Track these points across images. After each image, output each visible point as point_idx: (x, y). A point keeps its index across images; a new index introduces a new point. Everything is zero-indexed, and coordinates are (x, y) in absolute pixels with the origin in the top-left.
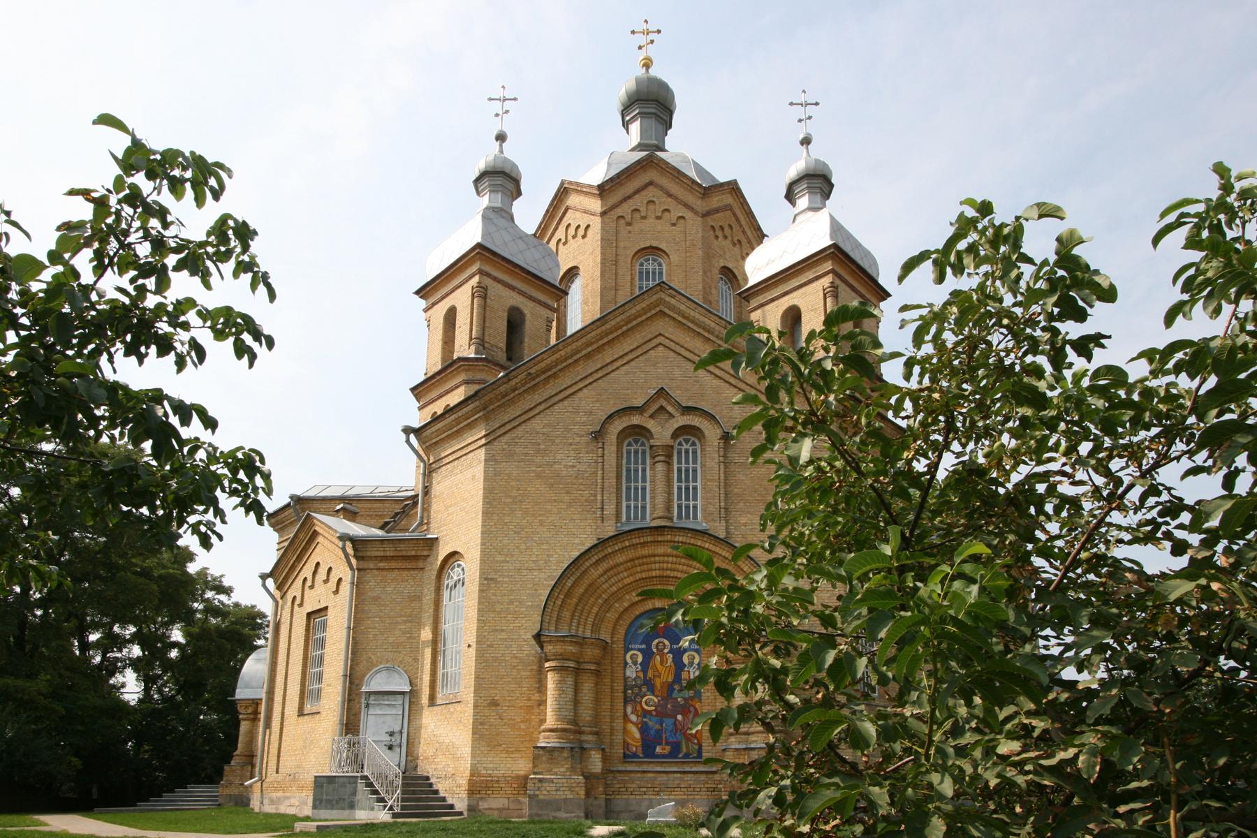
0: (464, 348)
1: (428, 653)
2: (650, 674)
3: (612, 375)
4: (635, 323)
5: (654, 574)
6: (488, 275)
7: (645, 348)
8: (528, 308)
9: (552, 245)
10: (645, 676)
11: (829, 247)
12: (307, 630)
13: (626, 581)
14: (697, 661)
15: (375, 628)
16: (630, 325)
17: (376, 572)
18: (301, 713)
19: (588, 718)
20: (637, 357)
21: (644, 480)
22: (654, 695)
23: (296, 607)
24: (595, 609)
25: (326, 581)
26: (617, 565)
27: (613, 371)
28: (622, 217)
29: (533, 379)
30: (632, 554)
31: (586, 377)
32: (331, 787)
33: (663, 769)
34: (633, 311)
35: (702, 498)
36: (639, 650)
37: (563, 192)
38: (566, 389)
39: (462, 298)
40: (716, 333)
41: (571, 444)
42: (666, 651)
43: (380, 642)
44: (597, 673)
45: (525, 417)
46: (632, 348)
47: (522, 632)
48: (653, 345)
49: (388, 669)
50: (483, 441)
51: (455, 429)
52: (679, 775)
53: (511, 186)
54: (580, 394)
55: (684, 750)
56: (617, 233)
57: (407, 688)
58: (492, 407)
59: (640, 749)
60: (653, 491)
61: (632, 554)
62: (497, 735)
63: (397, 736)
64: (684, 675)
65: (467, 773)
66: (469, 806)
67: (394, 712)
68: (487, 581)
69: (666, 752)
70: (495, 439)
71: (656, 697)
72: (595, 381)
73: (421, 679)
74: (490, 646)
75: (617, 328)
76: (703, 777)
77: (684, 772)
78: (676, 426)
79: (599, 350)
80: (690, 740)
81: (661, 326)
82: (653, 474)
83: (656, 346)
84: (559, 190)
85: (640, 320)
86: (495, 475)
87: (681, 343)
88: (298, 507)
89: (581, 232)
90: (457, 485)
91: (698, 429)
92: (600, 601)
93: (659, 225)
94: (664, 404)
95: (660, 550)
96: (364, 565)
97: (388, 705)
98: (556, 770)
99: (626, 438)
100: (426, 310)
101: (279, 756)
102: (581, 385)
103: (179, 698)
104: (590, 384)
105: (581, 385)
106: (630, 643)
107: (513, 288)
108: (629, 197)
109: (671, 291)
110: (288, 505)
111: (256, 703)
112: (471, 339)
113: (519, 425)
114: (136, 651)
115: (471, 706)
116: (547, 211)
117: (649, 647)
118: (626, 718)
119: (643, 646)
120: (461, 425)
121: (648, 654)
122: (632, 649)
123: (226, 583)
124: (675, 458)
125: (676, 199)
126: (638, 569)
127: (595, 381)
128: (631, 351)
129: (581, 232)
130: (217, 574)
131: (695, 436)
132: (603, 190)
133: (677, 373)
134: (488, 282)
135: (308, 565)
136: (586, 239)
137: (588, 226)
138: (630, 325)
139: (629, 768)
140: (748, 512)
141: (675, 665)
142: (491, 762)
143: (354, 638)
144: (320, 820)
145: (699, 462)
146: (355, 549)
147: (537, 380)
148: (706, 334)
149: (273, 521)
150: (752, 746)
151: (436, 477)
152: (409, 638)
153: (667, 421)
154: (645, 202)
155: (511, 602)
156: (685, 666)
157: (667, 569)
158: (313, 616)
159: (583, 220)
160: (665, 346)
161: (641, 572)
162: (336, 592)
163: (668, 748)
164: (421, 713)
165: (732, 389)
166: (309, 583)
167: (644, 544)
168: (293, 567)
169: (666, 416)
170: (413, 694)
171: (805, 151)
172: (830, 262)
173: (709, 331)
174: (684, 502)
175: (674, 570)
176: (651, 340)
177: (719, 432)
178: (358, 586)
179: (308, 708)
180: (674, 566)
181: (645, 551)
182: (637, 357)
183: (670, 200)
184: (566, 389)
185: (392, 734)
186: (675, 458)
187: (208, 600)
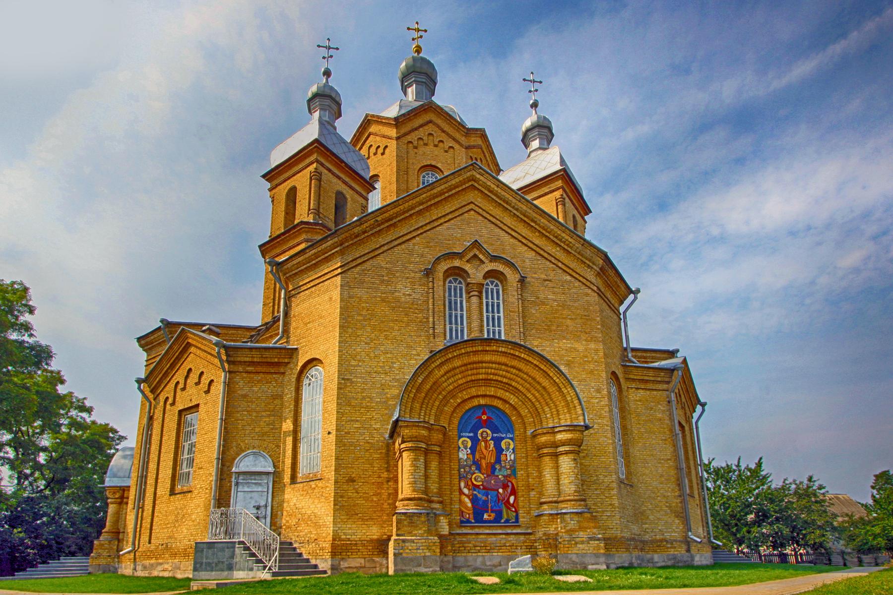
0: (303, 214)
1: (289, 440)
2: (477, 456)
3: (437, 229)
4: (454, 191)
5: (481, 377)
6: (322, 165)
7: (461, 211)
8: (349, 194)
9: (364, 152)
10: (474, 457)
11: (560, 171)
12: (179, 424)
13: (460, 382)
14: (512, 447)
15: (243, 420)
16: (451, 193)
17: (245, 375)
18: (172, 492)
19: (435, 490)
20: (455, 217)
21: (462, 310)
22: (480, 472)
23: (168, 407)
24: (437, 403)
25: (198, 384)
26: (454, 368)
27: (438, 226)
28: (411, 142)
29: (379, 225)
30: (466, 360)
31: (418, 229)
32: (210, 551)
33: (491, 532)
34: (453, 182)
35: (505, 325)
36: (468, 437)
37: (368, 122)
38: (403, 236)
39: (302, 181)
40: (513, 204)
41: (408, 278)
42: (489, 438)
43: (247, 432)
44: (440, 454)
45: (372, 255)
46: (451, 210)
47: (373, 422)
48: (467, 210)
49: (254, 453)
50: (339, 271)
51: (314, 262)
52: (504, 536)
53: (335, 107)
54: (414, 241)
55: (505, 516)
56: (408, 152)
57: (271, 469)
58: (347, 244)
59: (472, 516)
60: (469, 318)
61: (466, 360)
62: (354, 506)
63: (263, 509)
64: (503, 458)
65: (330, 538)
66: (332, 565)
67: (260, 489)
68: (344, 382)
69: (492, 518)
70: (348, 269)
71: (483, 474)
72: (425, 232)
73: (283, 462)
74: (348, 433)
75: (442, 193)
76: (522, 538)
77: (507, 534)
78: (486, 270)
79: (428, 209)
80: (510, 509)
81: (471, 196)
82: (467, 305)
83: (469, 211)
84: (364, 121)
85: (457, 190)
86: (350, 297)
87: (486, 210)
88: (167, 330)
89: (380, 151)
90: (315, 305)
91: (502, 273)
92: (440, 397)
93: (436, 151)
94: (477, 253)
95: (487, 358)
96: (235, 368)
97: (255, 484)
98: (416, 532)
99: (448, 277)
100: (270, 190)
101: (151, 529)
102: (415, 234)
103: (47, 492)
104: (421, 234)
105: (415, 234)
106: (461, 432)
107: (339, 178)
108: (416, 129)
109: (480, 170)
110: (159, 329)
111: (124, 490)
112: (309, 210)
113: (367, 260)
114: (11, 454)
115: (332, 482)
116: (355, 135)
117: (476, 434)
118: (461, 492)
119: (471, 434)
120: (319, 259)
121: (475, 441)
122: (463, 437)
123: (88, 404)
124: (484, 294)
125: (448, 134)
126: (470, 372)
127: (425, 232)
128: (451, 212)
129: (380, 151)
130: (81, 397)
131: (498, 279)
132: (398, 122)
133: (484, 231)
134: (321, 169)
135: (180, 371)
136: (384, 156)
137: (386, 147)
138: (451, 193)
139: (465, 531)
140: (539, 338)
141: (496, 449)
142: (350, 529)
143: (225, 428)
144: (218, 580)
145: (501, 298)
146: (228, 355)
147: (382, 227)
148: (505, 205)
149: (143, 342)
150: (563, 511)
151: (295, 302)
152: (272, 429)
153: (479, 266)
154: (427, 133)
155: (364, 398)
156: (503, 450)
157: (491, 374)
158: (184, 413)
159: (383, 142)
160: (475, 211)
161: (471, 375)
162: (208, 392)
163: (493, 515)
164: (283, 492)
165: (523, 247)
166: (181, 386)
167: (476, 352)
168: (166, 374)
169: (478, 263)
170: (277, 475)
171: (534, 111)
172: (560, 181)
173: (507, 203)
174: (491, 328)
175: (496, 375)
176: (465, 206)
177: (518, 277)
178: (229, 386)
179: (179, 488)
180: (496, 371)
181: (476, 359)
182: (455, 217)
183: (443, 134)
184: (403, 236)
185: (258, 508)
186: (484, 294)
187: (71, 417)
